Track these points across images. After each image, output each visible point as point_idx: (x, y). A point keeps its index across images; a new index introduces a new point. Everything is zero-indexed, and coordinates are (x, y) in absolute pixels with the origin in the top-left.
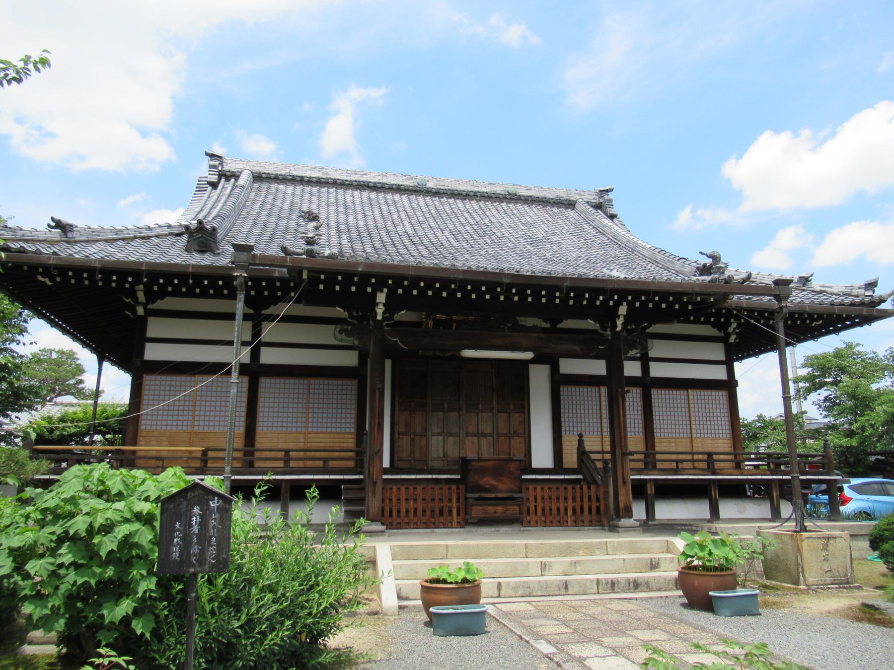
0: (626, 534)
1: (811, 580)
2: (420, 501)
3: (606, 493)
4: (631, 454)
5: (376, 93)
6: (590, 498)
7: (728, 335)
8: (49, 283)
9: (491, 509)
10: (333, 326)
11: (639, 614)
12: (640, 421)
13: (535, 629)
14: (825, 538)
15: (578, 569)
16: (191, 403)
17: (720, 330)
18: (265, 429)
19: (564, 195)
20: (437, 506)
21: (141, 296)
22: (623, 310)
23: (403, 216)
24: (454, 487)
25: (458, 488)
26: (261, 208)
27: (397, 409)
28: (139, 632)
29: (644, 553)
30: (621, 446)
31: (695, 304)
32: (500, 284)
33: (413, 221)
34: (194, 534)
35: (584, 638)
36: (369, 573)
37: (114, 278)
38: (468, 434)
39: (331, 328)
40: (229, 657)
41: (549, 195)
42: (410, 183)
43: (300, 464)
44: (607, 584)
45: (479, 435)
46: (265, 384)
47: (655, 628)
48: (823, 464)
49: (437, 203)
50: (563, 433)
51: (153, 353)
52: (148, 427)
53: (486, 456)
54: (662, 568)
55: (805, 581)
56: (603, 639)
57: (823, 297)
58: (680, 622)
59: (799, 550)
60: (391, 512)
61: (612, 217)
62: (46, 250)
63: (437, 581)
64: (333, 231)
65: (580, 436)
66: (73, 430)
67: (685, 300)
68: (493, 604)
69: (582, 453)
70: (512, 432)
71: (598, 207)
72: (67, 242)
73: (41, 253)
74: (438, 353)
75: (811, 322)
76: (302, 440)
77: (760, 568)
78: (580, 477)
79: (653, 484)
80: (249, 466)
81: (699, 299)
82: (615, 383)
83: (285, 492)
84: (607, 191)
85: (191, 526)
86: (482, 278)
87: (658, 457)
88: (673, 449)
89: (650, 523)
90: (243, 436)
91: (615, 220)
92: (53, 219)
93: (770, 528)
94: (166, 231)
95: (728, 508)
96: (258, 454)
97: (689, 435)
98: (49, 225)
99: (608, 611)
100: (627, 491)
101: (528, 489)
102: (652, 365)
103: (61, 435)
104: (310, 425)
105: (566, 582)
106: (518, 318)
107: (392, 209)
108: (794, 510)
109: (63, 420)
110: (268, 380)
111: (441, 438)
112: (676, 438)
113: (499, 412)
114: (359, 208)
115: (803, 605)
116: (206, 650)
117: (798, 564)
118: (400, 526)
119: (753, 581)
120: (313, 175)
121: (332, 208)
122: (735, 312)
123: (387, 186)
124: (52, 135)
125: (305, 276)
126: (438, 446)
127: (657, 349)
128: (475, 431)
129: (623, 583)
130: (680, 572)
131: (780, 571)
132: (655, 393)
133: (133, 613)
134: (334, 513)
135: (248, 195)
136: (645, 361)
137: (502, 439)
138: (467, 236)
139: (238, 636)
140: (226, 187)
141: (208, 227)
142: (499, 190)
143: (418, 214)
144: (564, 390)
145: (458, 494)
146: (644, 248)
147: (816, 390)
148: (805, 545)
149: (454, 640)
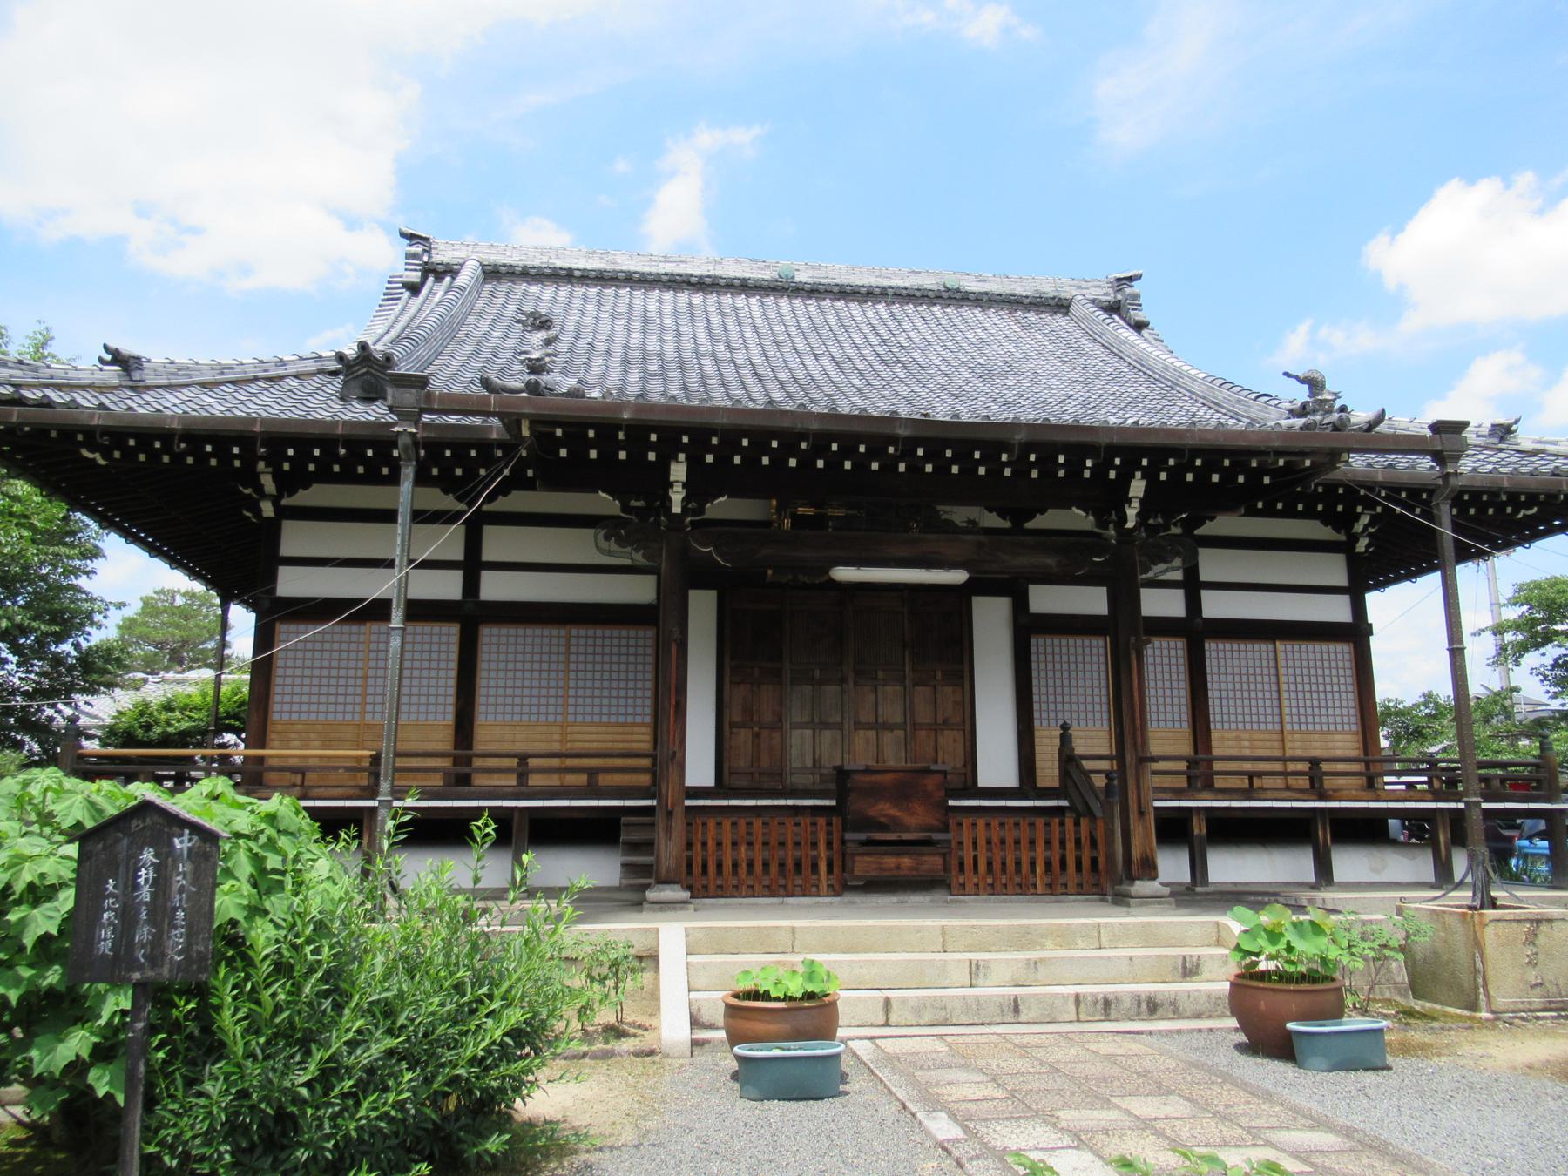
0: (1143, 910)
1: (1501, 1001)
2: (758, 846)
3: (1110, 833)
4: (1154, 759)
5: (743, 137)
6: (1078, 842)
7: (1354, 539)
8: (102, 462)
9: (890, 861)
10: (592, 531)
11: (1147, 1064)
12: (1184, 701)
13: (933, 1090)
14: (1531, 921)
15: (1042, 972)
16: (360, 673)
17: (1337, 530)
18: (490, 717)
19: (1049, 290)
20: (790, 855)
21: (268, 483)
22: (1138, 487)
23: (749, 333)
24: (822, 821)
25: (829, 824)
26: (492, 326)
27: (727, 680)
28: (101, 1093)
29: (1167, 947)
30: (1135, 745)
31: (1275, 473)
32: (893, 440)
33: (766, 342)
34: (141, 903)
35: (1022, 1107)
36: (647, 977)
37: (236, 450)
38: (858, 725)
39: (588, 533)
40: (285, 1141)
41: (1020, 290)
42: (766, 275)
43: (554, 781)
44: (1096, 1002)
45: (880, 726)
46: (492, 638)
47: (1170, 1093)
48: (1538, 781)
49: (812, 309)
50: (1037, 723)
51: (292, 583)
52: (286, 717)
53: (891, 763)
54: (1205, 975)
55: (1489, 1003)
56: (1061, 1114)
57: (1537, 462)
58: (1224, 1081)
59: (1478, 944)
60: (705, 866)
61: (1139, 326)
62: (86, 400)
63: (755, 995)
64: (616, 362)
65: (1065, 727)
66: (185, 725)
67: (1254, 464)
68: (872, 1038)
69: (1068, 759)
70: (940, 721)
71: (1113, 308)
72: (132, 388)
73: (78, 406)
74: (801, 578)
75: (1516, 511)
76: (557, 737)
77: (1402, 977)
78: (1064, 803)
79: (1203, 817)
80: (460, 781)
81: (1281, 462)
82: (1124, 632)
83: (520, 829)
84: (1130, 279)
85: (136, 887)
86: (857, 428)
87: (1217, 766)
88: (1247, 753)
89: (1199, 889)
90: (451, 731)
91: (1145, 332)
92: (106, 348)
93: (1423, 901)
94: (312, 366)
95: (1350, 863)
96: (478, 763)
97: (1278, 727)
98: (101, 360)
99: (1088, 1056)
100: (1146, 828)
101: (960, 824)
102: (1206, 595)
103: (164, 732)
104: (571, 710)
105: (1016, 1000)
106: (939, 508)
107: (730, 322)
108: (1470, 867)
109: (168, 707)
110: (495, 631)
111: (808, 732)
112: (1252, 732)
113: (916, 684)
114: (668, 322)
115: (1480, 1051)
116: (233, 1129)
117: (1476, 971)
118: (721, 892)
119: (1388, 1002)
120: (589, 267)
121: (621, 322)
122: (1362, 492)
123: (722, 282)
124: (195, 231)
125: (525, 432)
126: (804, 748)
127: (1212, 565)
128: (872, 720)
129: (1127, 1005)
130: (1232, 984)
131: (1441, 983)
132: (1212, 649)
133: (91, 1056)
134: (591, 869)
135: (472, 305)
136: (1193, 587)
137: (922, 734)
138: (861, 366)
139: (297, 1100)
140: (436, 291)
141: (379, 356)
142: (929, 282)
143: (777, 329)
144: (1038, 643)
145: (829, 833)
146: (1193, 379)
147: (1537, 646)
148: (1490, 935)
149: (776, 1107)
